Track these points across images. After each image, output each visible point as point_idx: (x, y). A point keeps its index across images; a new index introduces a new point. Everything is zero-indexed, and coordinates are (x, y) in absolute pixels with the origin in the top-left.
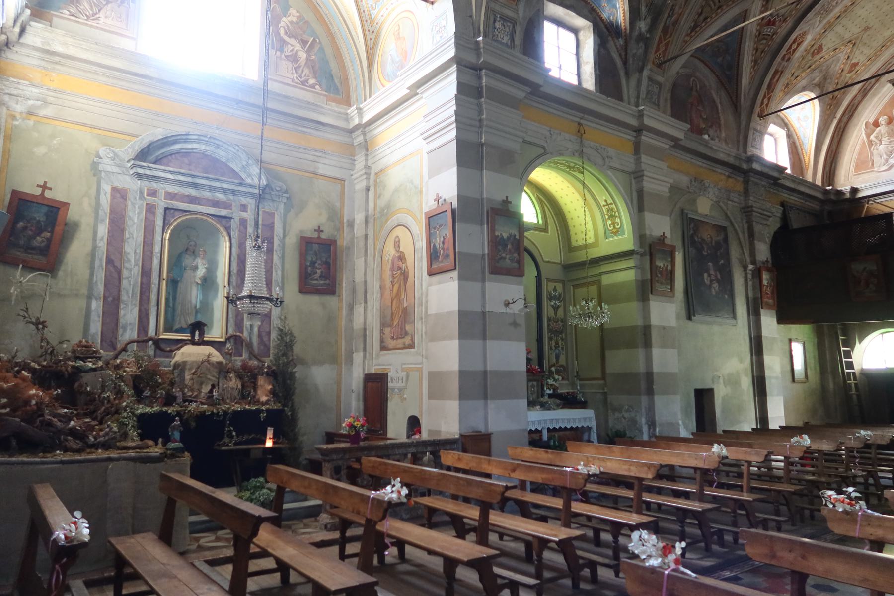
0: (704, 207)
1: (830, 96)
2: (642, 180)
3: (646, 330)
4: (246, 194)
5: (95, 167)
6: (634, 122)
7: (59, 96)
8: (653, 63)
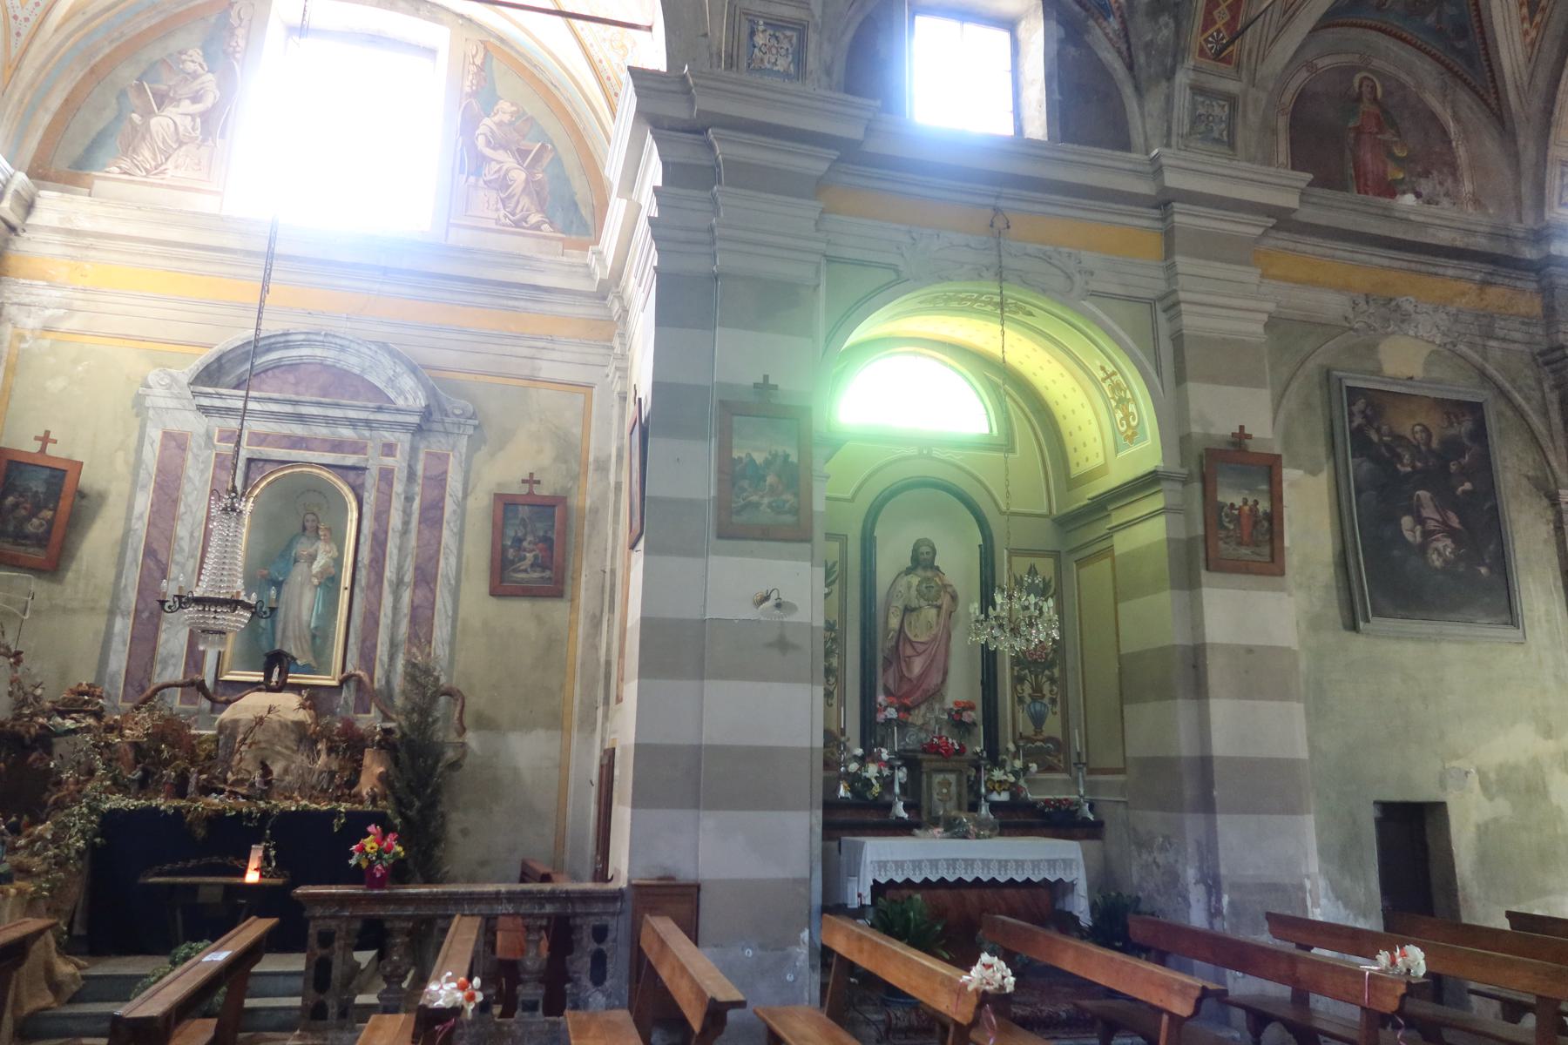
0: (1404, 359)
2: (1179, 314)
3: (1195, 659)
4: (392, 426)
5: (139, 405)
6: (1144, 188)
7: (91, 297)
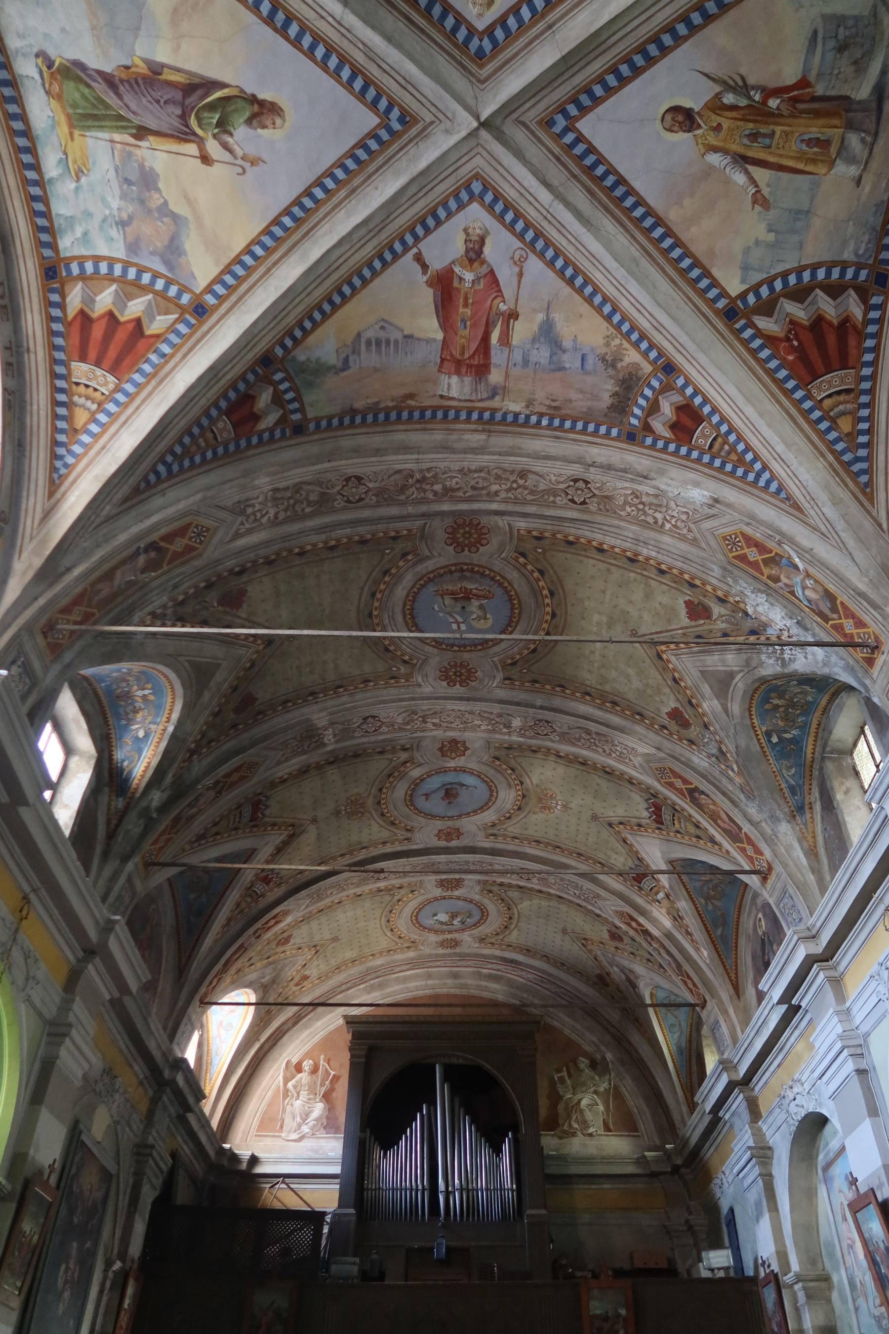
1: (267, 1007)
2: (60, 1044)
8: (143, 858)
